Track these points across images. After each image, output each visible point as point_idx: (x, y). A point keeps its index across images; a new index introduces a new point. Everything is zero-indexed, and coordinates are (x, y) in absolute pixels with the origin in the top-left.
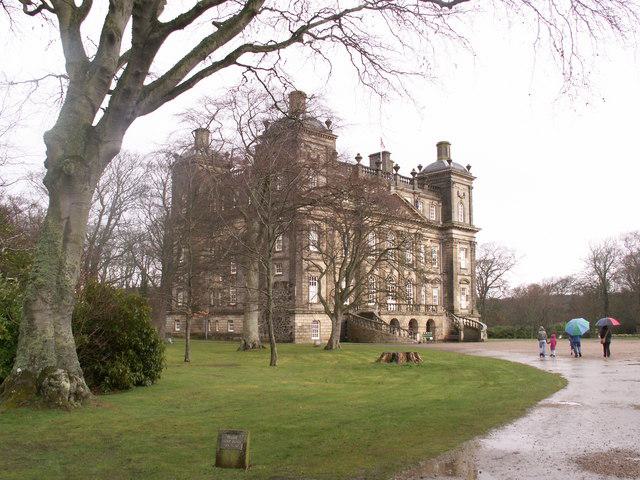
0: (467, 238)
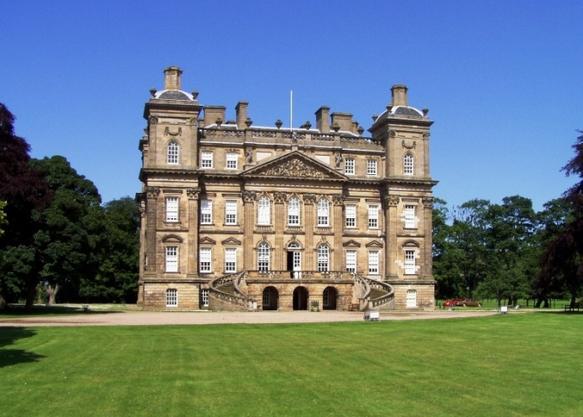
0: (416, 194)
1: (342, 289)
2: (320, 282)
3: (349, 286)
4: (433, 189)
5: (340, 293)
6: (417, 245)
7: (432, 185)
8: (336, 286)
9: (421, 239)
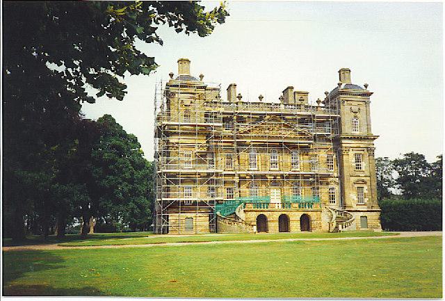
1: (313, 216)
2: (298, 211)
4: (375, 142)
5: (312, 219)
6: (365, 183)
7: (375, 139)
8: (309, 213)
9: (368, 178)
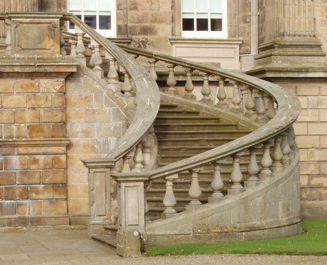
3: (50, 86)
